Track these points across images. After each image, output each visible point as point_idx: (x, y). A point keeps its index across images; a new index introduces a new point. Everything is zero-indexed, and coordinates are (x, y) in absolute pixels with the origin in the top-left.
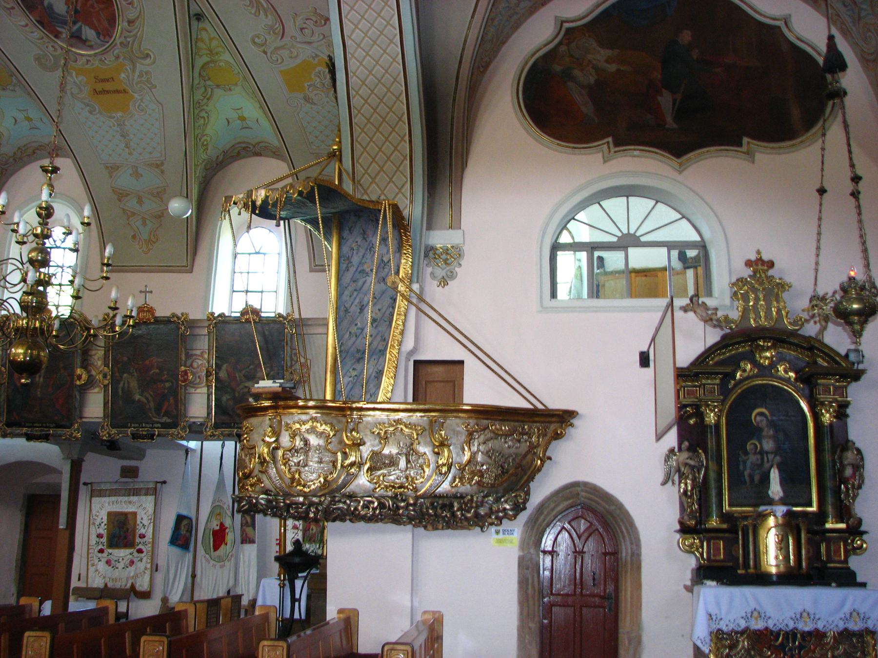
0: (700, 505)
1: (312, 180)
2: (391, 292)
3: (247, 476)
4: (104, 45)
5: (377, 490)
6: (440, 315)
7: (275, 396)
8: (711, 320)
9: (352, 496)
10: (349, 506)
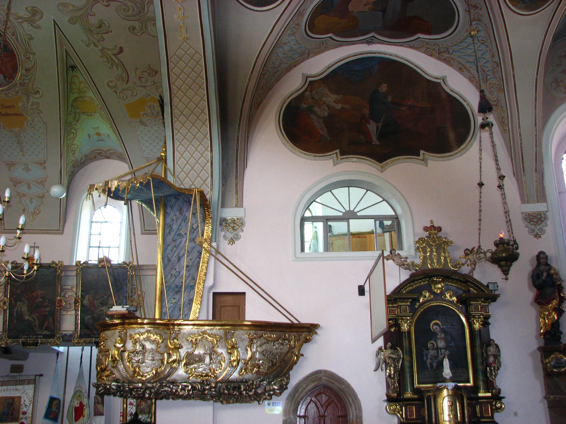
0: (399, 384)
1: (149, 175)
2: (198, 248)
3: (103, 370)
4: (9, 84)
5: (191, 378)
6: (231, 263)
7: (122, 317)
8: (404, 265)
9: (174, 382)
10: (172, 389)
